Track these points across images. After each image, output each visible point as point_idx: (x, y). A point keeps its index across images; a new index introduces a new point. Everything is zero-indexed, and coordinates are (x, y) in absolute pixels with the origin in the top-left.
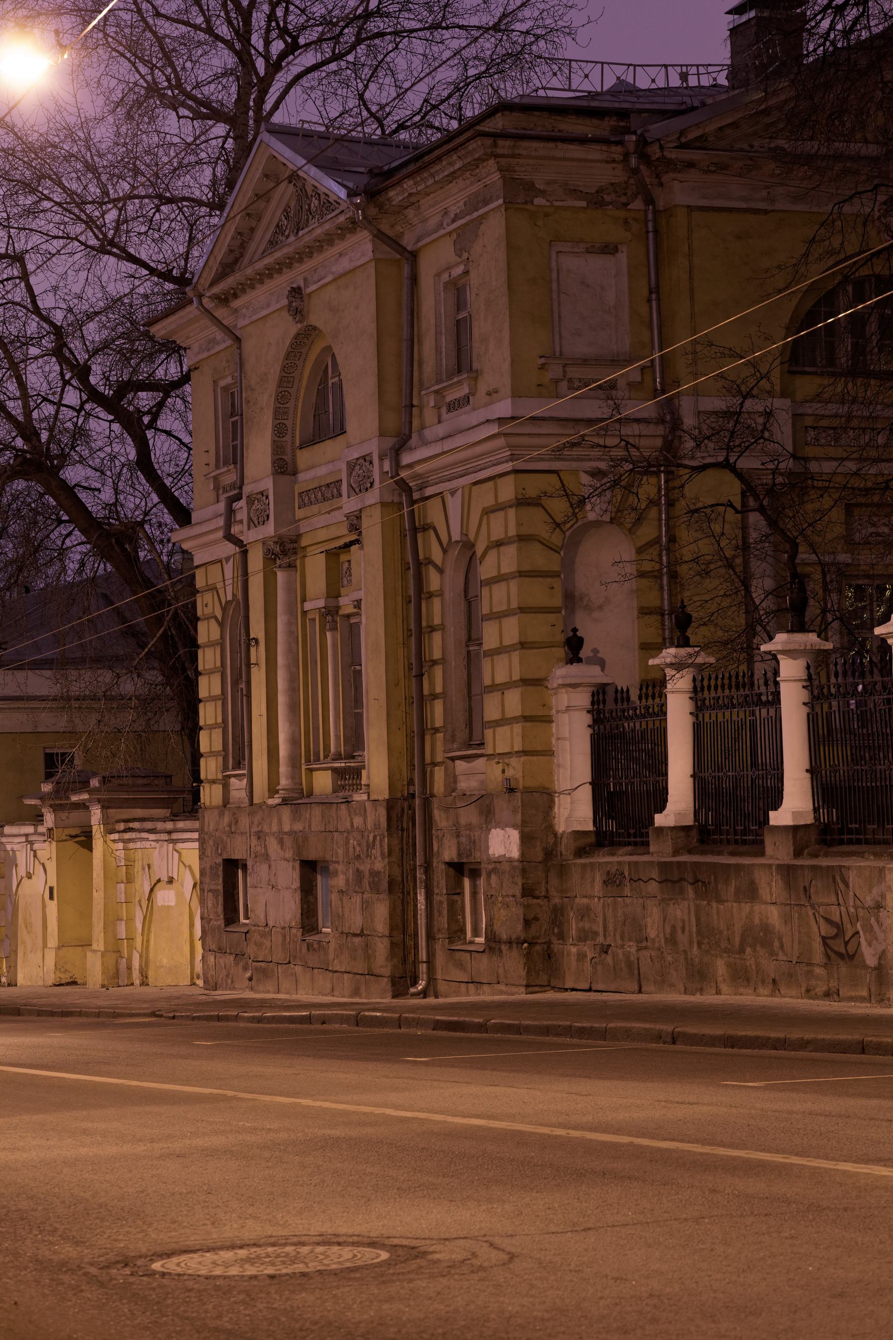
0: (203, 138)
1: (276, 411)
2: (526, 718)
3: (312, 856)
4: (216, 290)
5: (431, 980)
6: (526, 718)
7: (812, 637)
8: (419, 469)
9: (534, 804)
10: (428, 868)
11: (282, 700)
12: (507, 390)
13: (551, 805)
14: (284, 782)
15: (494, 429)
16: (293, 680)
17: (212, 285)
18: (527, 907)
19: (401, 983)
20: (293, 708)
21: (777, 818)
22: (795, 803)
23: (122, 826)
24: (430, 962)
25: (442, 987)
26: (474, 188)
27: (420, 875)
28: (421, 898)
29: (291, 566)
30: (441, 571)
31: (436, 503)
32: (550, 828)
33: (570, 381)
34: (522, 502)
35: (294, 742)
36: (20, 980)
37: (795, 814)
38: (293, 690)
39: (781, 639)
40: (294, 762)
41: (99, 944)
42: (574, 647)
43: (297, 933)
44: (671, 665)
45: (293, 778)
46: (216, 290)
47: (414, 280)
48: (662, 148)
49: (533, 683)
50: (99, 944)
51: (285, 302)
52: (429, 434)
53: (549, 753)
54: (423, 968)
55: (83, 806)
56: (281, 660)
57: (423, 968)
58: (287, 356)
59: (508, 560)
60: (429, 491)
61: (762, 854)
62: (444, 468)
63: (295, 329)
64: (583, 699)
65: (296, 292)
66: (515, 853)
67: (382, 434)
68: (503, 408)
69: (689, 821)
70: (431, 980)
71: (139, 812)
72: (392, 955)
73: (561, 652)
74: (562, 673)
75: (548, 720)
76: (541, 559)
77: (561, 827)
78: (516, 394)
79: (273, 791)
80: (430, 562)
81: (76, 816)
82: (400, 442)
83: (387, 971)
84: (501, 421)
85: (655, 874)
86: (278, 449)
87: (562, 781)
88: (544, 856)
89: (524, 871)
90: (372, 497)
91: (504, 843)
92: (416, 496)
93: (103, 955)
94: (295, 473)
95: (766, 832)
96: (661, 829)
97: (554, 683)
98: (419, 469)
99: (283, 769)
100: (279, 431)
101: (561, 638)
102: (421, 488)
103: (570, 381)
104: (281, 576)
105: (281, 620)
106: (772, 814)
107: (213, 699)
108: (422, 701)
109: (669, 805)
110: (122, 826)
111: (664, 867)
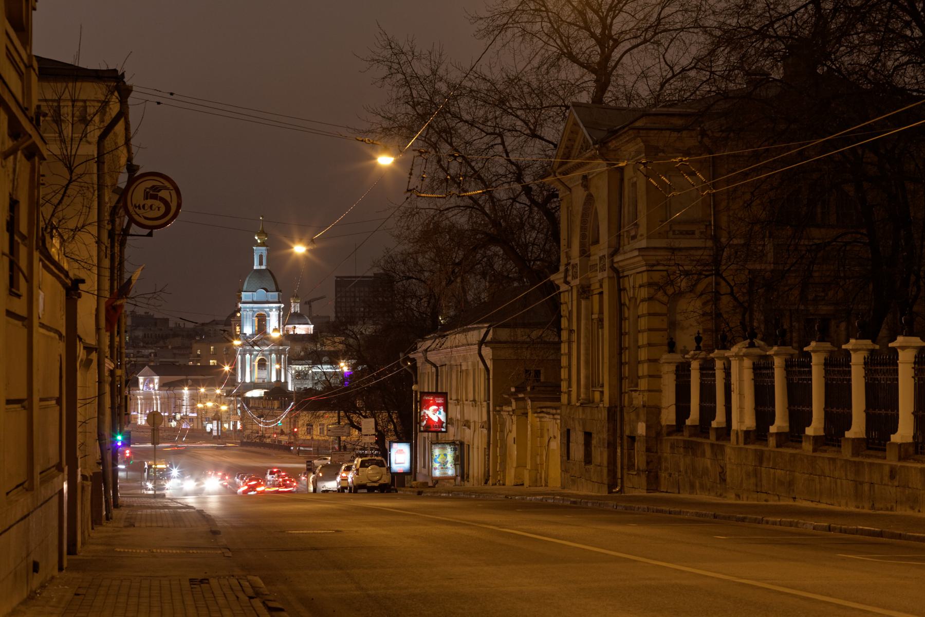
0: (581, 81)
1: (581, 228)
2: (650, 376)
3: (588, 430)
4: (559, 170)
5: (622, 487)
6: (650, 376)
7: (869, 342)
8: (621, 264)
9: (654, 411)
10: (622, 438)
11: (582, 358)
12: (645, 235)
13: (660, 413)
14: (582, 396)
15: (636, 253)
16: (587, 349)
17: (559, 167)
18: (648, 456)
19: (611, 486)
20: (587, 362)
21: (848, 434)
22: (905, 432)
23: (539, 410)
24: (622, 478)
25: (626, 489)
26: (637, 147)
27: (618, 441)
28: (619, 450)
29: (587, 298)
30: (629, 309)
31: (626, 279)
32: (659, 423)
33: (674, 231)
34: (650, 285)
35: (587, 378)
36: (507, 483)
37: (856, 433)
38: (587, 354)
39: (900, 340)
40: (587, 387)
41: (529, 467)
42: (671, 347)
43: (583, 464)
44: (852, 350)
45: (586, 394)
46: (559, 170)
47: (622, 180)
48: (712, 132)
49: (653, 361)
50: (529, 467)
51: (581, 181)
52: (627, 248)
53: (660, 391)
54: (619, 481)
55: (523, 399)
56: (582, 341)
57: (619, 481)
58: (585, 204)
59: (643, 308)
60: (625, 274)
61: (708, 438)
62: (633, 264)
63: (586, 193)
64: (673, 368)
65: (585, 177)
66: (644, 434)
67: (609, 247)
68: (643, 244)
69: (697, 423)
70: (622, 487)
71: (548, 404)
72: (609, 475)
73: (666, 348)
74: (666, 357)
75: (660, 377)
76: (658, 308)
77: (663, 423)
78: (649, 238)
79: (578, 400)
80: (625, 304)
81: (521, 404)
82: (615, 252)
83: (606, 482)
84: (640, 250)
85: (682, 444)
86: (582, 245)
87: (665, 403)
88: (656, 433)
89: (647, 441)
90: (605, 274)
91: (641, 429)
92: (621, 275)
93: (530, 471)
94: (589, 256)
95: (888, 448)
96: (848, 439)
97: (662, 361)
98: (621, 264)
99: (582, 390)
100: (583, 237)
101: (666, 342)
102: (623, 272)
103: (674, 231)
104: (583, 302)
105: (583, 322)
106: (892, 436)
107: (565, 354)
108: (621, 364)
109: (813, 424)
110: (539, 410)
111: (685, 441)
